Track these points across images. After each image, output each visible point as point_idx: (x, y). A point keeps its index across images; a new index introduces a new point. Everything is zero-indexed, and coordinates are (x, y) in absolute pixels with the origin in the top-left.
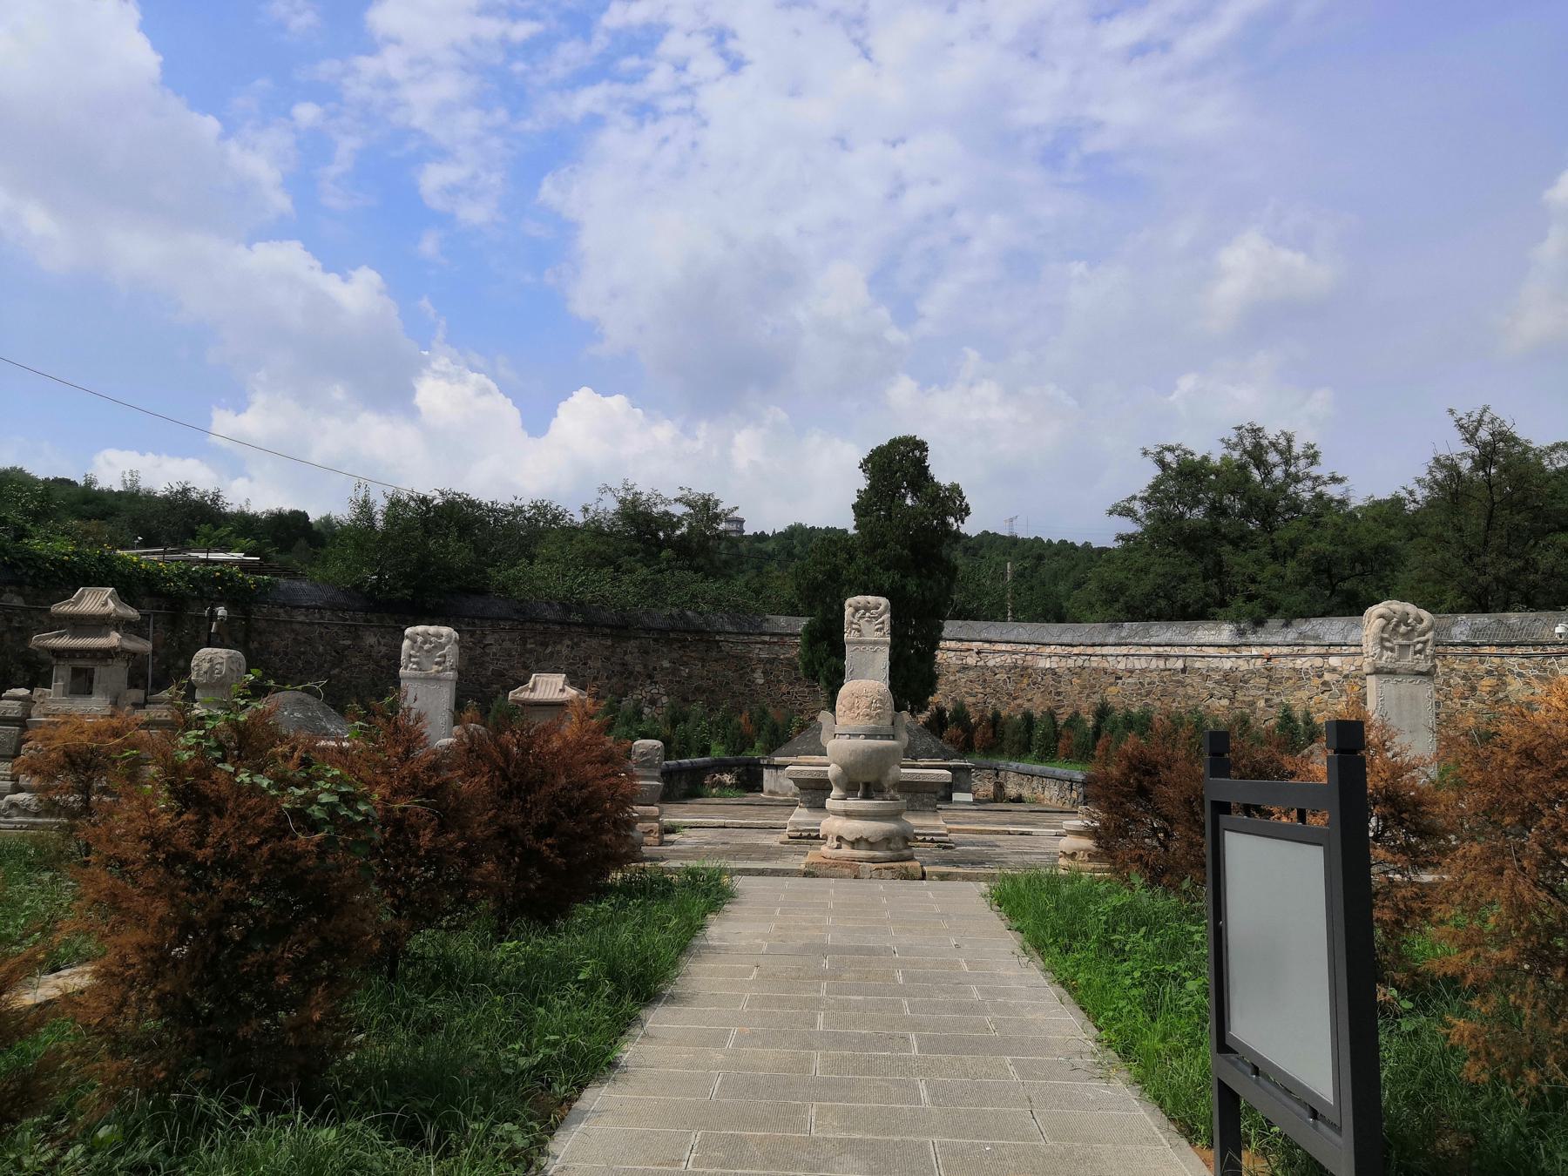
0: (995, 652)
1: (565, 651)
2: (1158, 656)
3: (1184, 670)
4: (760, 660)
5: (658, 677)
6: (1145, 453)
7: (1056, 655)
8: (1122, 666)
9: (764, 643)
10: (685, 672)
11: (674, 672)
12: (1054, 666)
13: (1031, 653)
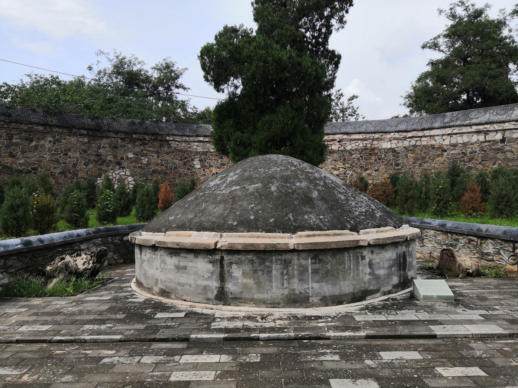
0: (351, 140)
1: (48, 145)
2: (478, 132)
3: (503, 141)
4: (197, 153)
5: (125, 164)
6: (441, 12)
7: (395, 139)
8: (447, 142)
9: (200, 141)
10: (145, 160)
11: (137, 160)
12: (394, 146)
13: (377, 139)
